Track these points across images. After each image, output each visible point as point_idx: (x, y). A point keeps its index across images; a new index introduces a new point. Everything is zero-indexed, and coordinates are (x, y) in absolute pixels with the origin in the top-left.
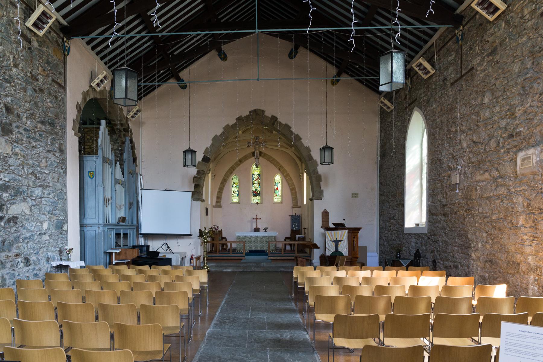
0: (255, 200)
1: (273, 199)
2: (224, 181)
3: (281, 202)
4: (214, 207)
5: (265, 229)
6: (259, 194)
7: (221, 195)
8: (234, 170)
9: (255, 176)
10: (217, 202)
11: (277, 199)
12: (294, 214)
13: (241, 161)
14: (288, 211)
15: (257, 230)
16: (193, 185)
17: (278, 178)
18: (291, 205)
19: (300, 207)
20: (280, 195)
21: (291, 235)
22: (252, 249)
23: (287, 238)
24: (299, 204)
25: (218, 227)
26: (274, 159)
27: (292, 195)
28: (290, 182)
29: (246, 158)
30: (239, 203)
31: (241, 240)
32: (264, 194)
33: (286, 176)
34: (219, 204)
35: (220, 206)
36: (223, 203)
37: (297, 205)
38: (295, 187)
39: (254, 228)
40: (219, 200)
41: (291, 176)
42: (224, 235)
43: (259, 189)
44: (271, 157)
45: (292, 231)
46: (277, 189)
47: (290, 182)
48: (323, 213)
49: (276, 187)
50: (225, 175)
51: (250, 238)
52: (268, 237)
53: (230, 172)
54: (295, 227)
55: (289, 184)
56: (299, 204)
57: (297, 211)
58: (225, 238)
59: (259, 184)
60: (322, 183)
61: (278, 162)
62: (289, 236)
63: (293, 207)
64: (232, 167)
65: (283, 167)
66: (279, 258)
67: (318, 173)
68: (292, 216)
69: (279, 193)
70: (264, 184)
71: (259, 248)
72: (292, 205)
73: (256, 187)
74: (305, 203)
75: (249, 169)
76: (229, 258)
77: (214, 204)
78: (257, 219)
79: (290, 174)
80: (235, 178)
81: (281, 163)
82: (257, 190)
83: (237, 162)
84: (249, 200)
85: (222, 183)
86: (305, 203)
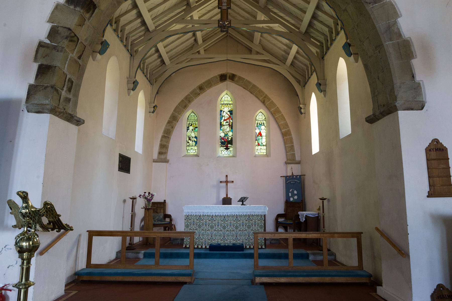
0: (223, 152)
1: (253, 149)
2: (174, 119)
3: (268, 155)
4: (154, 161)
5: (242, 200)
6: (231, 142)
7: (168, 142)
8: (190, 102)
9: (224, 114)
10: (160, 153)
11: (261, 151)
12: (289, 174)
13: (201, 88)
14: (278, 169)
15: (227, 201)
16: (35, 67)
17: (261, 116)
18: (283, 158)
19: (299, 163)
20: (264, 144)
21: (286, 210)
22: (215, 242)
23: (279, 216)
24: (298, 158)
25: (152, 195)
26: (254, 86)
27: (285, 143)
28: (282, 123)
29: (209, 84)
30: (197, 156)
31: (198, 220)
32: (238, 143)
33: (274, 112)
34: (162, 157)
35: (166, 161)
36: (170, 155)
37: (294, 159)
38: (289, 131)
39: (221, 199)
40: (163, 151)
41: (283, 113)
42: (169, 212)
43: (230, 134)
44: (250, 83)
45: (288, 203)
46: (260, 134)
47: (282, 123)
48: (428, 150)
49: (257, 131)
50: (175, 110)
51: (212, 218)
52: (249, 217)
53: (184, 105)
54: (293, 195)
55: (279, 126)
56: (298, 158)
57: (295, 170)
58: (169, 216)
59: (231, 126)
60: (416, 63)
61: (260, 91)
62: (283, 212)
63: (286, 163)
64: (186, 98)
65: (269, 99)
66: (283, 280)
67: (400, 35)
68: (286, 177)
69: (263, 140)
70: (238, 126)
71: (230, 241)
72: (285, 160)
73: (225, 131)
74: (315, 148)
75: (213, 102)
76: (150, 279)
77: (155, 156)
78: (227, 182)
79: (281, 109)
80: (189, 114)
81: (266, 91)
82: (226, 135)
83: (194, 90)
84: (215, 151)
85: (169, 122)
86: (315, 148)
